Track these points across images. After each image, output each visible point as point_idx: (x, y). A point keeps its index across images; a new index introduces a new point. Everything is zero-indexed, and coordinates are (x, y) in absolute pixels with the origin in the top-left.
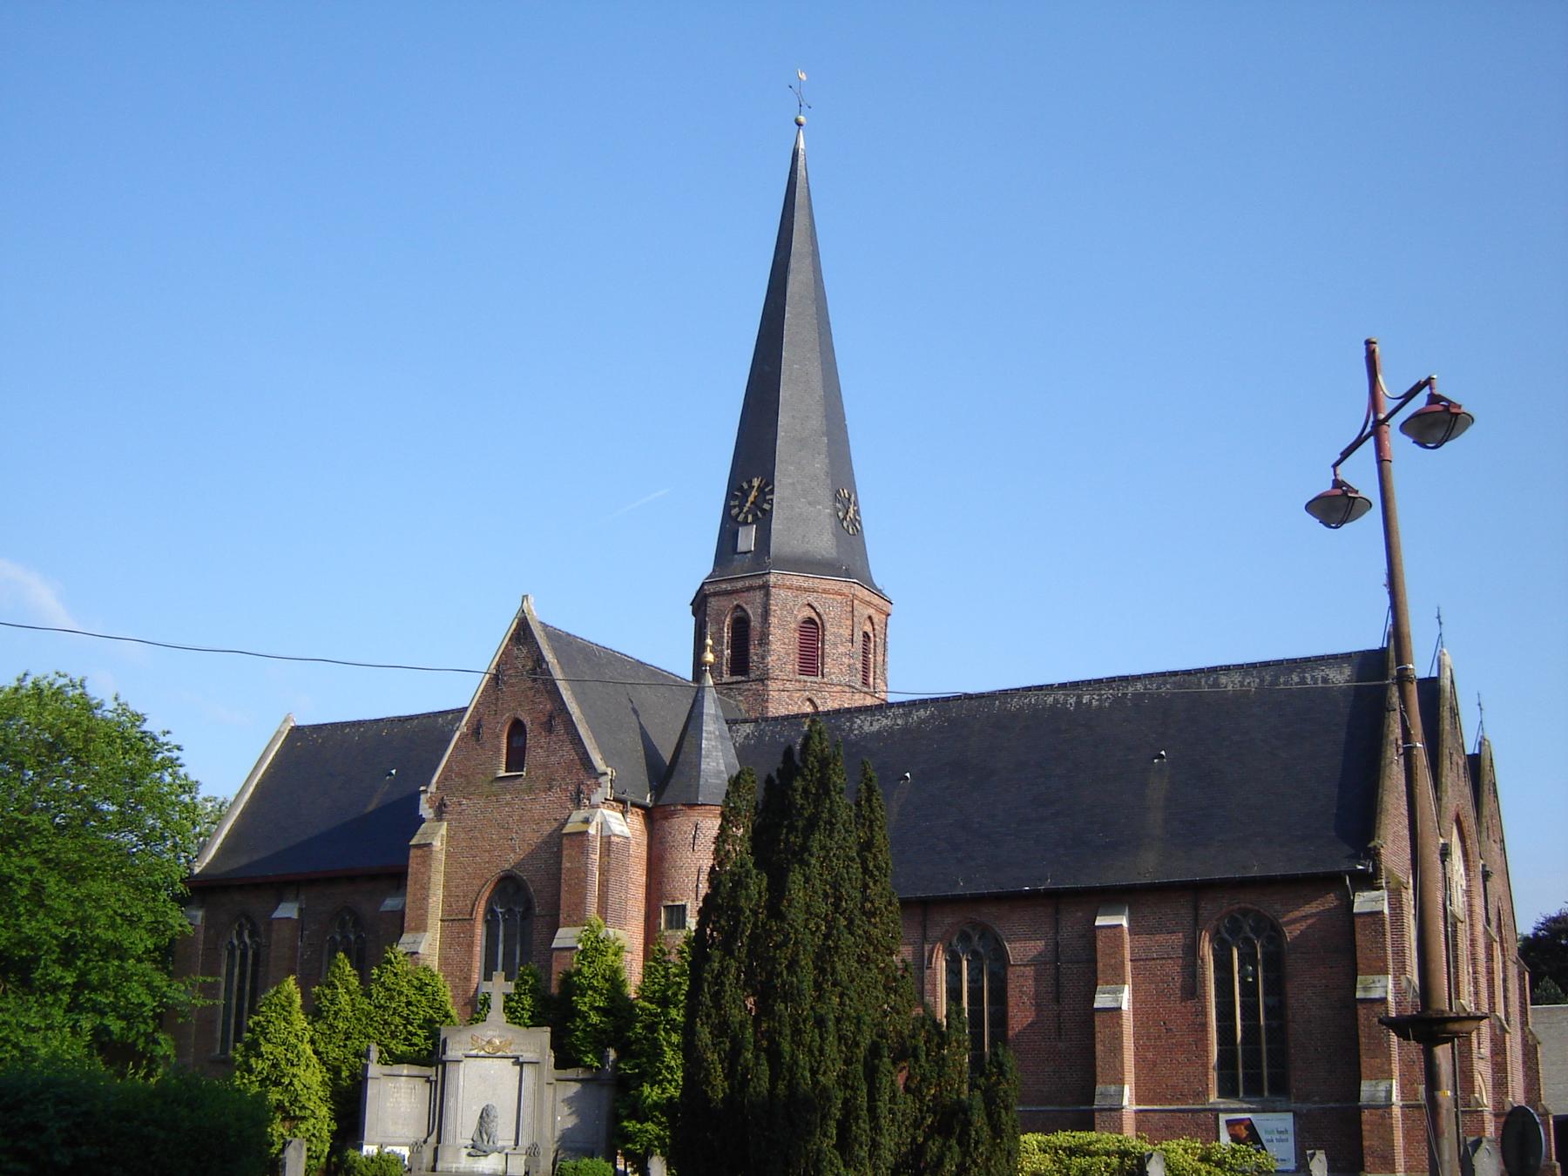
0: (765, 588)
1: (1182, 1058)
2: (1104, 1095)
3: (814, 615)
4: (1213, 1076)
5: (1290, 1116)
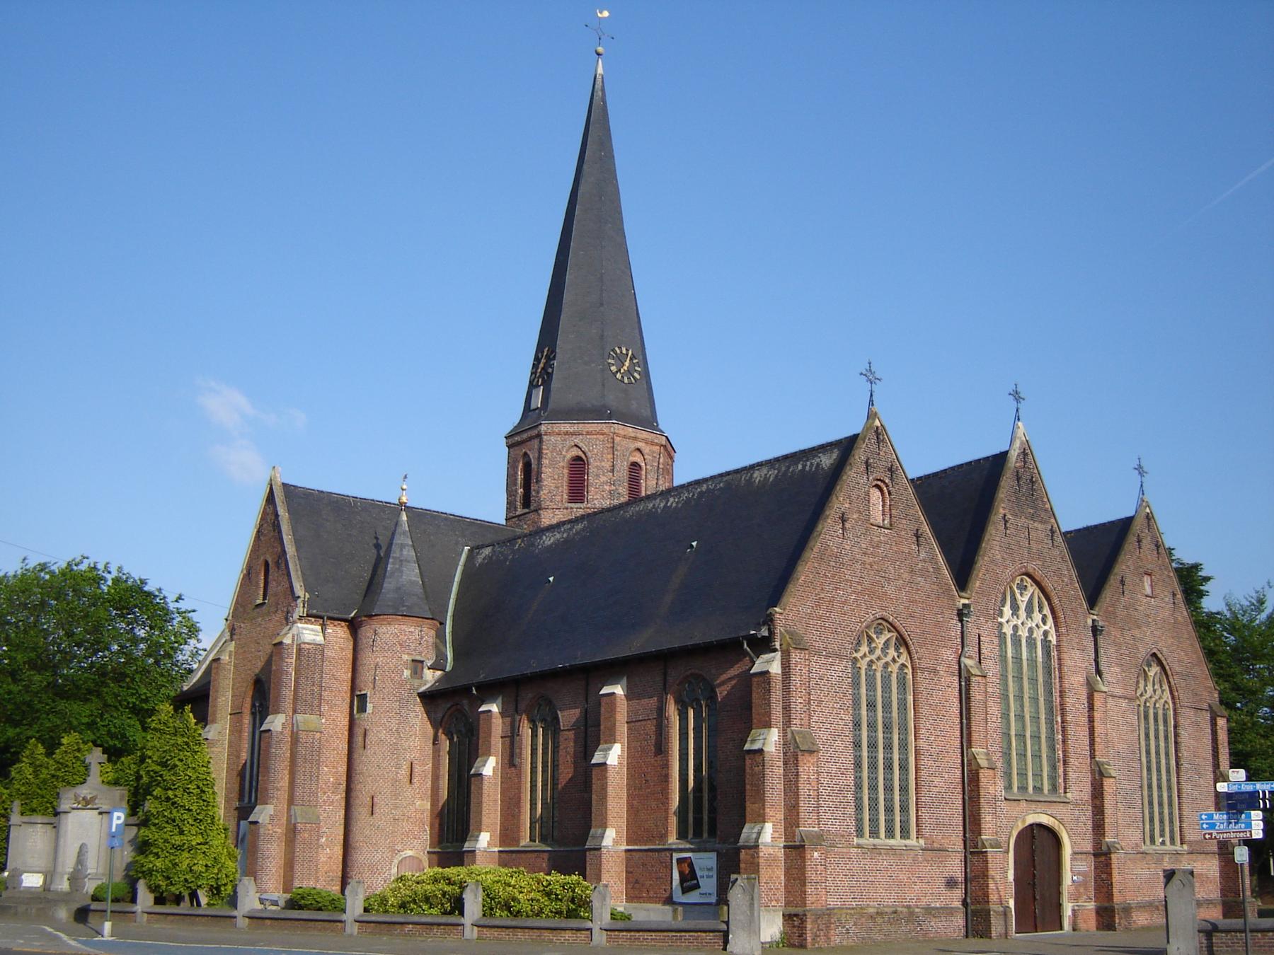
0: (539, 436)
1: (653, 805)
2: (594, 837)
3: (581, 454)
4: (673, 821)
5: (714, 855)
